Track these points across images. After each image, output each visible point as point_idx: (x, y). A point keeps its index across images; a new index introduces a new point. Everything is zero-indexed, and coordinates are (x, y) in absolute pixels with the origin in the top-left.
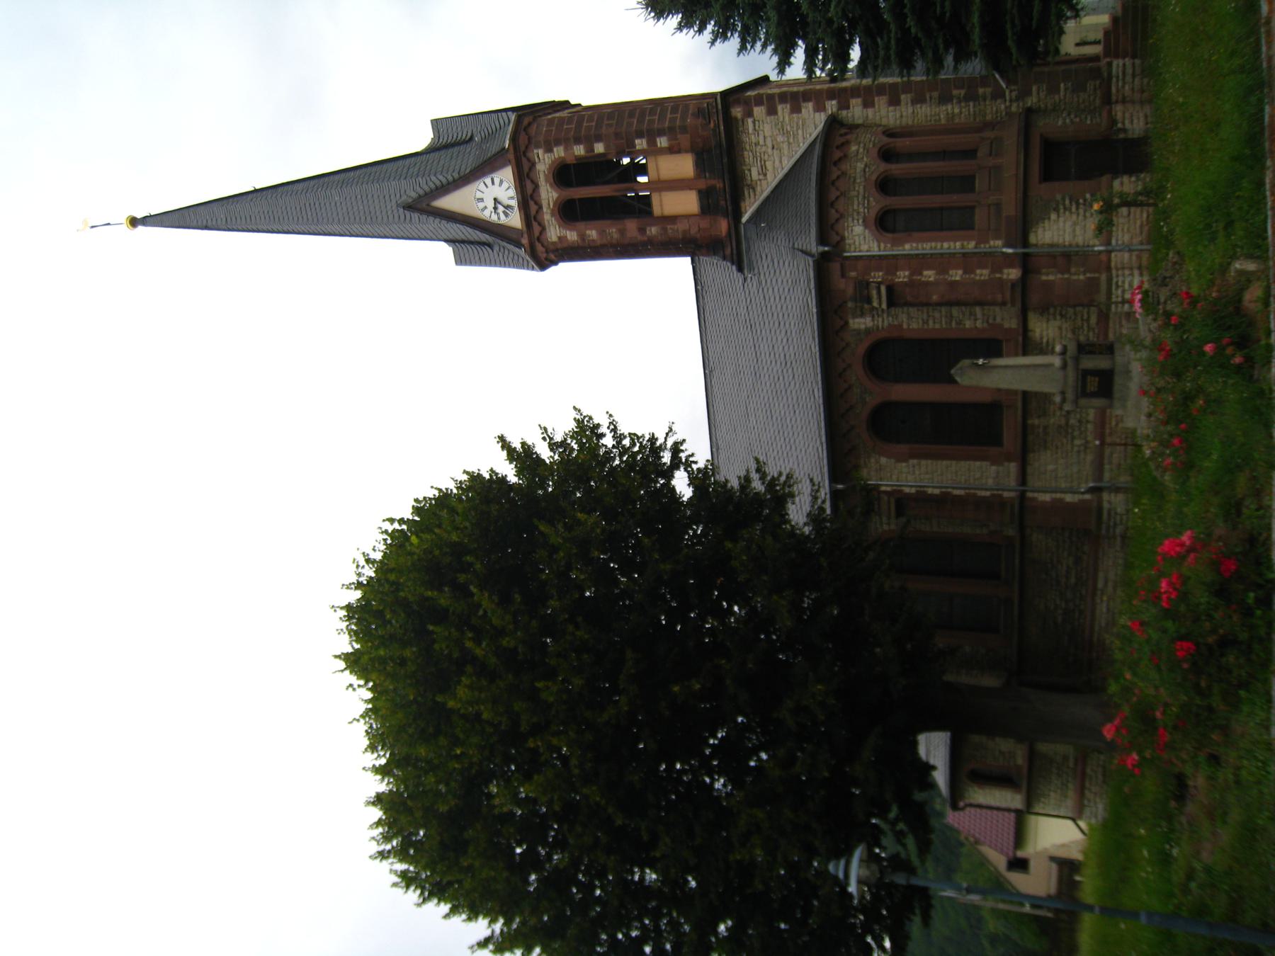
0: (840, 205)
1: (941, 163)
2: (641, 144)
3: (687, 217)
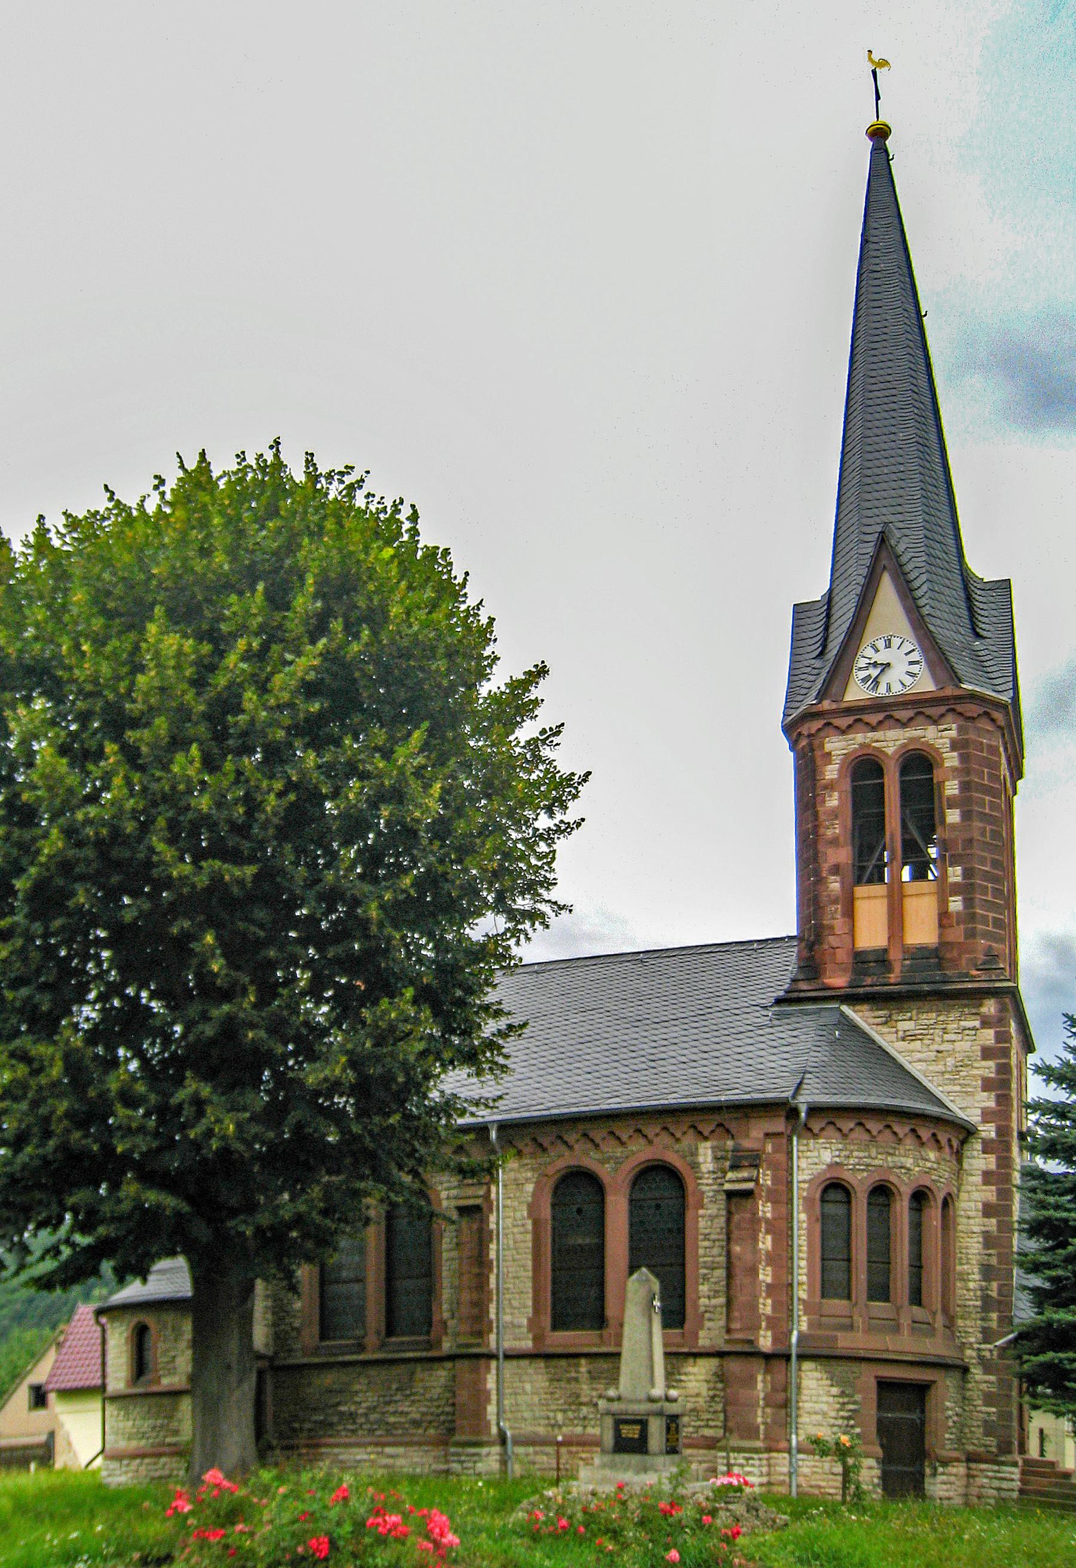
0: (859, 1134)
1: (906, 1262)
2: (955, 874)
3: (852, 933)
